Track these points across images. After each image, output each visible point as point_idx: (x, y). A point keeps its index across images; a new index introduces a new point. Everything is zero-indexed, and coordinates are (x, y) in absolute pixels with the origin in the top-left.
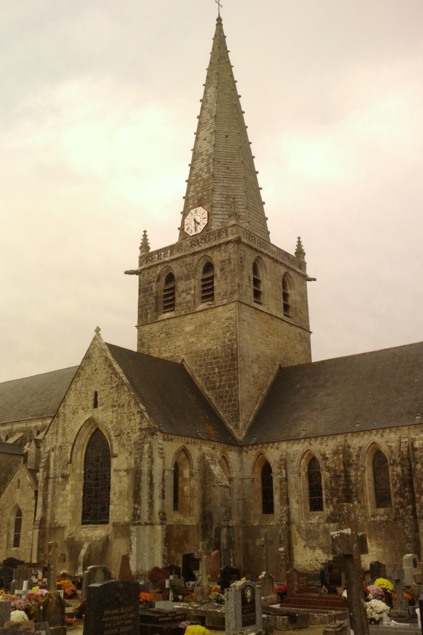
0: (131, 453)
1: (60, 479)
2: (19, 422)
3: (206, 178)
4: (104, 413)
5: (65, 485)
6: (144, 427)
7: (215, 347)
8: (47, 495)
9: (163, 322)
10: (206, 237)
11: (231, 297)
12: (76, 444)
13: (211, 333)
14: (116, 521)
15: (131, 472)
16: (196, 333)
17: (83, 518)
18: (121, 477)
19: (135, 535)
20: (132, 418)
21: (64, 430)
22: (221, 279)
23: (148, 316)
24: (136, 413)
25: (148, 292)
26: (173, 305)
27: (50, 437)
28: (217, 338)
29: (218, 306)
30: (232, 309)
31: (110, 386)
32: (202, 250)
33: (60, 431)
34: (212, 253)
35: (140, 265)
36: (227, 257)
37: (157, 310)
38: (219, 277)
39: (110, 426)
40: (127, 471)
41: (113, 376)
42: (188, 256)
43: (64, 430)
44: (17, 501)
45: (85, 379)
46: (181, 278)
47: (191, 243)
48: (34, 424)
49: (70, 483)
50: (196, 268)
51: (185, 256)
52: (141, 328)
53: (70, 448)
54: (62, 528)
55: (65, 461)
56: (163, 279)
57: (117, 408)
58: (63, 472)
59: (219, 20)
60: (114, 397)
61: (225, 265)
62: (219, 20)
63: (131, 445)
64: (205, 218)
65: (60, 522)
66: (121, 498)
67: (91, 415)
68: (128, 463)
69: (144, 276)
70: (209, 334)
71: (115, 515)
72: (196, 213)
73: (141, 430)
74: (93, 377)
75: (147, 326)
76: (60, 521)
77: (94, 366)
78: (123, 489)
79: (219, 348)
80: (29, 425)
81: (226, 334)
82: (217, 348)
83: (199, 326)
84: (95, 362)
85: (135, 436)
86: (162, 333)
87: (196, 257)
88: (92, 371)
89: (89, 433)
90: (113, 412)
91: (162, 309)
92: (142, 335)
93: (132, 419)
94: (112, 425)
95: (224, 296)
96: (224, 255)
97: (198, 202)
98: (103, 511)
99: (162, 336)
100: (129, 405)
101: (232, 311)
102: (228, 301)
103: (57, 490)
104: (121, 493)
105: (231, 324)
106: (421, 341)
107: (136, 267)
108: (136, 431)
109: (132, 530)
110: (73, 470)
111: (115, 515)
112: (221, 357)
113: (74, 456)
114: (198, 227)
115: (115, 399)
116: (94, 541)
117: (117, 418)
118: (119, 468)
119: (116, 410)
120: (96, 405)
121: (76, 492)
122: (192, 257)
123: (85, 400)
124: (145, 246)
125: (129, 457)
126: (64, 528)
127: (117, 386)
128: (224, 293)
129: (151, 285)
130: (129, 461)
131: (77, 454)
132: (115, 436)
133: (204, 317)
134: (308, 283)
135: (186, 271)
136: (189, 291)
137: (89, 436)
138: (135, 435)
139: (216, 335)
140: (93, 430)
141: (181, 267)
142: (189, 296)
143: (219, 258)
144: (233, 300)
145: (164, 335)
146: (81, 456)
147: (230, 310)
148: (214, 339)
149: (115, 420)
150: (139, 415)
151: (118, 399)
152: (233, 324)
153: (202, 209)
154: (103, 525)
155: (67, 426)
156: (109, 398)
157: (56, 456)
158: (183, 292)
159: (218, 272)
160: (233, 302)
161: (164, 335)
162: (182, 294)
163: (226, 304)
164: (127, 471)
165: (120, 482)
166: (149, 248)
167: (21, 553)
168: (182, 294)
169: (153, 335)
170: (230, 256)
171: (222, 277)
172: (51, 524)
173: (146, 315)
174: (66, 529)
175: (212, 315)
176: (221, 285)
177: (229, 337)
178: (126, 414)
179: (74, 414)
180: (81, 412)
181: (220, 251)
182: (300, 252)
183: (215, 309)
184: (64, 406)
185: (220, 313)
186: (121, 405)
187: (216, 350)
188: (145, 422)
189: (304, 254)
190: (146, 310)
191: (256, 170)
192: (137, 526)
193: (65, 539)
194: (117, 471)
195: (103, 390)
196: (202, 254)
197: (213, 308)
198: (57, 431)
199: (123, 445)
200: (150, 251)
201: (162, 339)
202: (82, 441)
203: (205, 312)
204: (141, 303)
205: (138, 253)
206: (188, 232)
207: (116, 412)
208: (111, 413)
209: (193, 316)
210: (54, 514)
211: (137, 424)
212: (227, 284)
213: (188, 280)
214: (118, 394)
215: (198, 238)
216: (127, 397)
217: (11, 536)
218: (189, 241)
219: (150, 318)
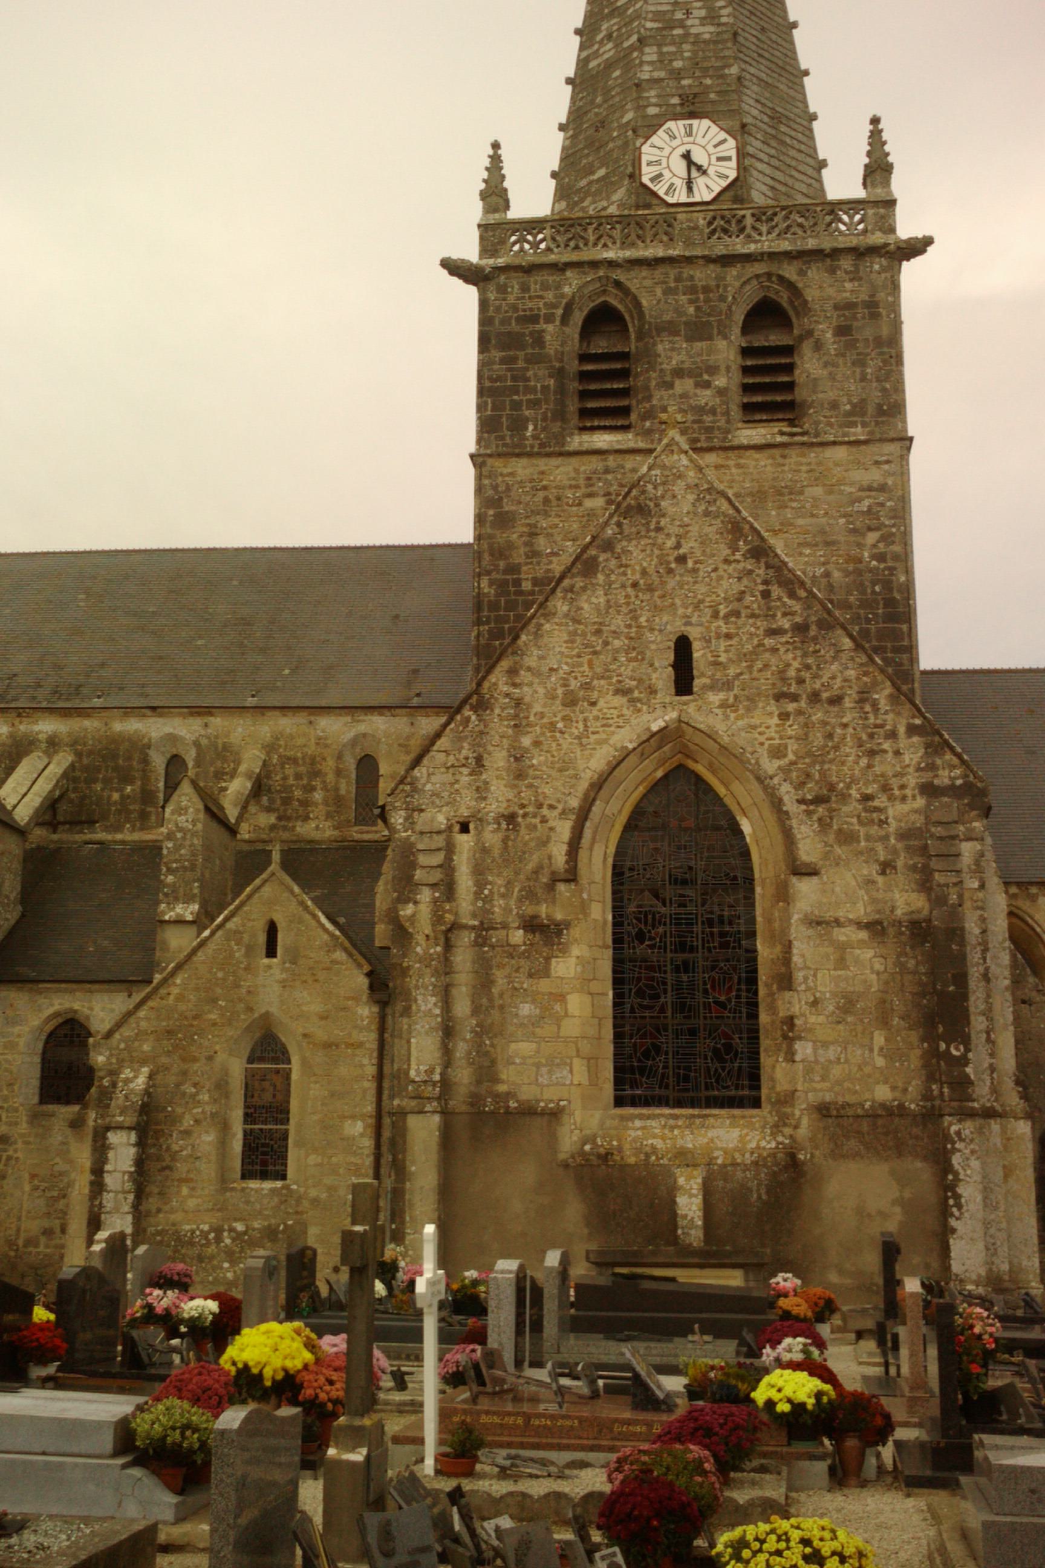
1: (518, 936)
3: (707, 36)
4: (741, 717)
5: (548, 959)
6: (947, 781)
7: (820, 571)
9: (594, 459)
10: (775, 214)
11: (883, 422)
12: (591, 815)
13: (800, 522)
14: (828, 1099)
15: (891, 931)
17: (618, 1082)
18: (842, 948)
19: (973, 1152)
20: (886, 746)
21: (517, 759)
22: (841, 361)
23: (527, 429)
24: (902, 730)
25: (522, 347)
26: (625, 411)
27: (441, 778)
28: (828, 544)
29: (834, 443)
30: (888, 462)
31: (762, 624)
32: (762, 254)
33: (498, 759)
34: (802, 273)
36: (864, 297)
37: (560, 415)
38: (833, 352)
39: (770, 766)
40: (875, 928)
41: (776, 591)
42: (701, 262)
43: (518, 756)
45: (623, 586)
46: (670, 328)
47: (710, 223)
48: (155, 728)
49: (576, 951)
50: (730, 307)
51: (689, 260)
52: (497, 464)
53: (564, 829)
54: (543, 1114)
55: (536, 872)
56: (578, 317)
57: (803, 704)
58: (529, 909)
60: (788, 665)
61: (854, 318)
63: (886, 837)
64: (729, 159)
65: (527, 1093)
66: (849, 1019)
67: (674, 715)
68: (874, 901)
69: (502, 290)
70: (791, 524)
71: (824, 1079)
72: (690, 135)
73: (929, 790)
74: (671, 583)
75: (524, 461)
76: (525, 1088)
77: (670, 543)
78: (860, 988)
79: (836, 574)
81: (864, 535)
82: (827, 574)
83: (751, 494)
84: (674, 530)
85: (905, 810)
86: (590, 495)
87: (734, 272)
88: (662, 561)
89: (645, 779)
90: (784, 716)
91: (576, 417)
92: (502, 488)
93: (885, 751)
94: (777, 763)
95: (849, 414)
96: (848, 286)
97: (682, 105)
98: (721, 1060)
99: (589, 503)
100: (864, 697)
101: (886, 467)
102: (871, 433)
104: (848, 1004)
105: (882, 505)
106: (1042, 666)
108: (908, 792)
109: (958, 1133)
110: (584, 908)
111: (824, 1079)
112: (845, 606)
113: (583, 855)
114: (700, 182)
115: (792, 673)
116: (724, 1166)
117: (803, 738)
118: (829, 915)
119: (800, 712)
120: (683, 683)
121: (595, 987)
122: (713, 270)
123: (630, 660)
125: (880, 879)
126: (555, 1115)
127: (801, 629)
128: (854, 406)
129: (538, 327)
130: (880, 895)
131: (591, 849)
132: (801, 801)
133: (769, 468)
135: (691, 310)
136: (706, 377)
137: (641, 789)
138: (905, 808)
139: (823, 532)
140: (659, 774)
141: (668, 291)
142: (708, 392)
143: (831, 291)
144: (892, 434)
146: (605, 859)
147: (877, 463)
148: (816, 545)
149: (792, 746)
150: (915, 739)
151: (806, 675)
152: (892, 509)
153: (715, 129)
154: (737, 1112)
155: (537, 743)
156: (759, 665)
158: (679, 373)
159: (829, 335)
160: (892, 440)
162: (677, 383)
163: (865, 442)
164: (875, 928)
165: (841, 963)
167: (305, 1203)
168: (677, 383)
169: (552, 494)
170: (872, 296)
171: (843, 355)
172: (475, 1100)
173: (518, 425)
174: (565, 1118)
175: (804, 468)
176: (839, 377)
177: (874, 546)
178: (850, 730)
179: (571, 701)
180: (610, 703)
181: (832, 271)
183: (818, 449)
184: (513, 672)
185: (837, 465)
186: (825, 695)
187: (824, 581)
188: (953, 767)
190: (516, 406)
191: (803, 67)
192: (979, 1121)
193: (562, 1156)
194: (819, 923)
195: (728, 636)
196: (759, 268)
197: (812, 445)
198: (479, 760)
200: (513, 214)
202: (613, 807)
203: (776, 452)
204: (491, 379)
205: (475, 211)
206: (661, 190)
207: (801, 719)
208: (775, 720)
209: (727, 458)
210: (493, 1062)
211: (911, 770)
212: (863, 379)
213: (701, 339)
214: (805, 655)
215: (742, 213)
216: (852, 673)
217: (235, 1135)
218: (701, 215)
219: (535, 437)
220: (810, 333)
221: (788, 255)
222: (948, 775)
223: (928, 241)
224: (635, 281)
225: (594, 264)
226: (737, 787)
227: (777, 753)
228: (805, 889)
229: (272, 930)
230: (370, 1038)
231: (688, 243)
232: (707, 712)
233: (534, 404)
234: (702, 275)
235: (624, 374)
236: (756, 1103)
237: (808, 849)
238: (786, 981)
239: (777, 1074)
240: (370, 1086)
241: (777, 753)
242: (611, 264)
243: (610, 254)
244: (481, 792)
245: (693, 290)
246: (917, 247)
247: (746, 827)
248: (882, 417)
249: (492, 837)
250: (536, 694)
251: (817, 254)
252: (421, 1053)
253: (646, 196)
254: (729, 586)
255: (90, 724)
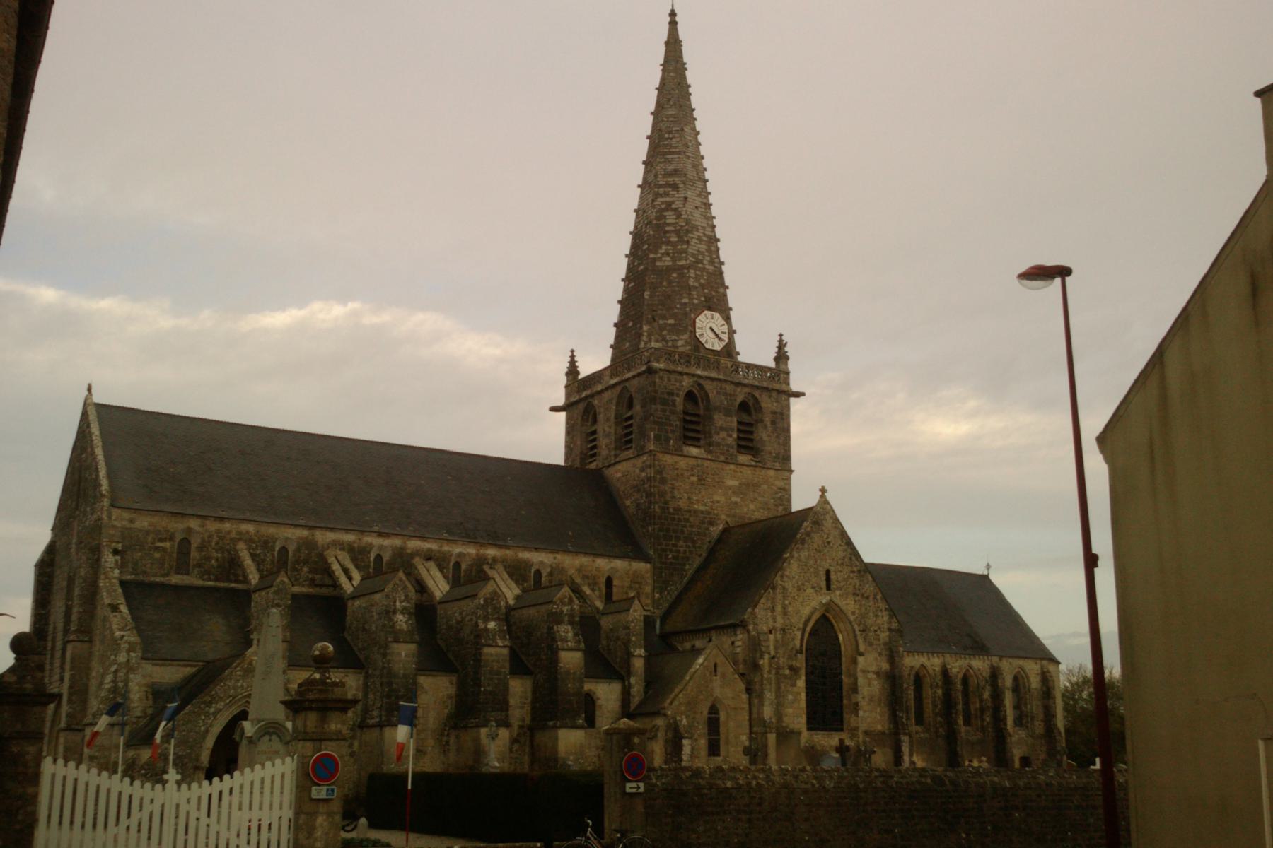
0: (880, 654)
1: (787, 672)
2: (423, 538)
8: (718, 741)
16: (738, 491)
27: (763, 613)
33: (779, 608)
35: (568, 395)
39: (852, 618)
40: (878, 674)
43: (784, 607)
44: (717, 692)
51: (725, 381)
59: (673, 14)
62: (673, 14)
65: (791, 726)
73: (890, 630)
80: (446, 548)
103: (782, 685)
107: (560, 400)
124: (572, 371)
127: (859, 571)
134: (792, 400)
145: (694, 479)
157: (776, 641)
161: (694, 479)
165: (869, 685)
166: (578, 373)
173: (667, 440)
182: (781, 356)
184: (782, 577)
189: (787, 358)
199: (871, 644)
201: (692, 483)
220: (762, 421)
221: (758, 387)
222: (895, 625)
223: (803, 394)
224: (709, 386)
225: (694, 375)
226: (841, 625)
227: (853, 613)
228: (861, 659)
229: (715, 665)
230: (746, 706)
231: (725, 374)
232: (836, 596)
233: (673, 431)
234: (729, 388)
235: (698, 423)
236: (842, 730)
237: (862, 648)
238: (855, 690)
239: (850, 719)
240: (747, 723)
241: (853, 613)
242: (700, 377)
243: (699, 372)
244: (774, 620)
245: (726, 394)
246: (798, 395)
247: (841, 637)
248: (784, 459)
249: (779, 636)
250: (789, 585)
251: (767, 389)
252: (768, 712)
253: (697, 344)
254: (841, 554)
255: (509, 552)
